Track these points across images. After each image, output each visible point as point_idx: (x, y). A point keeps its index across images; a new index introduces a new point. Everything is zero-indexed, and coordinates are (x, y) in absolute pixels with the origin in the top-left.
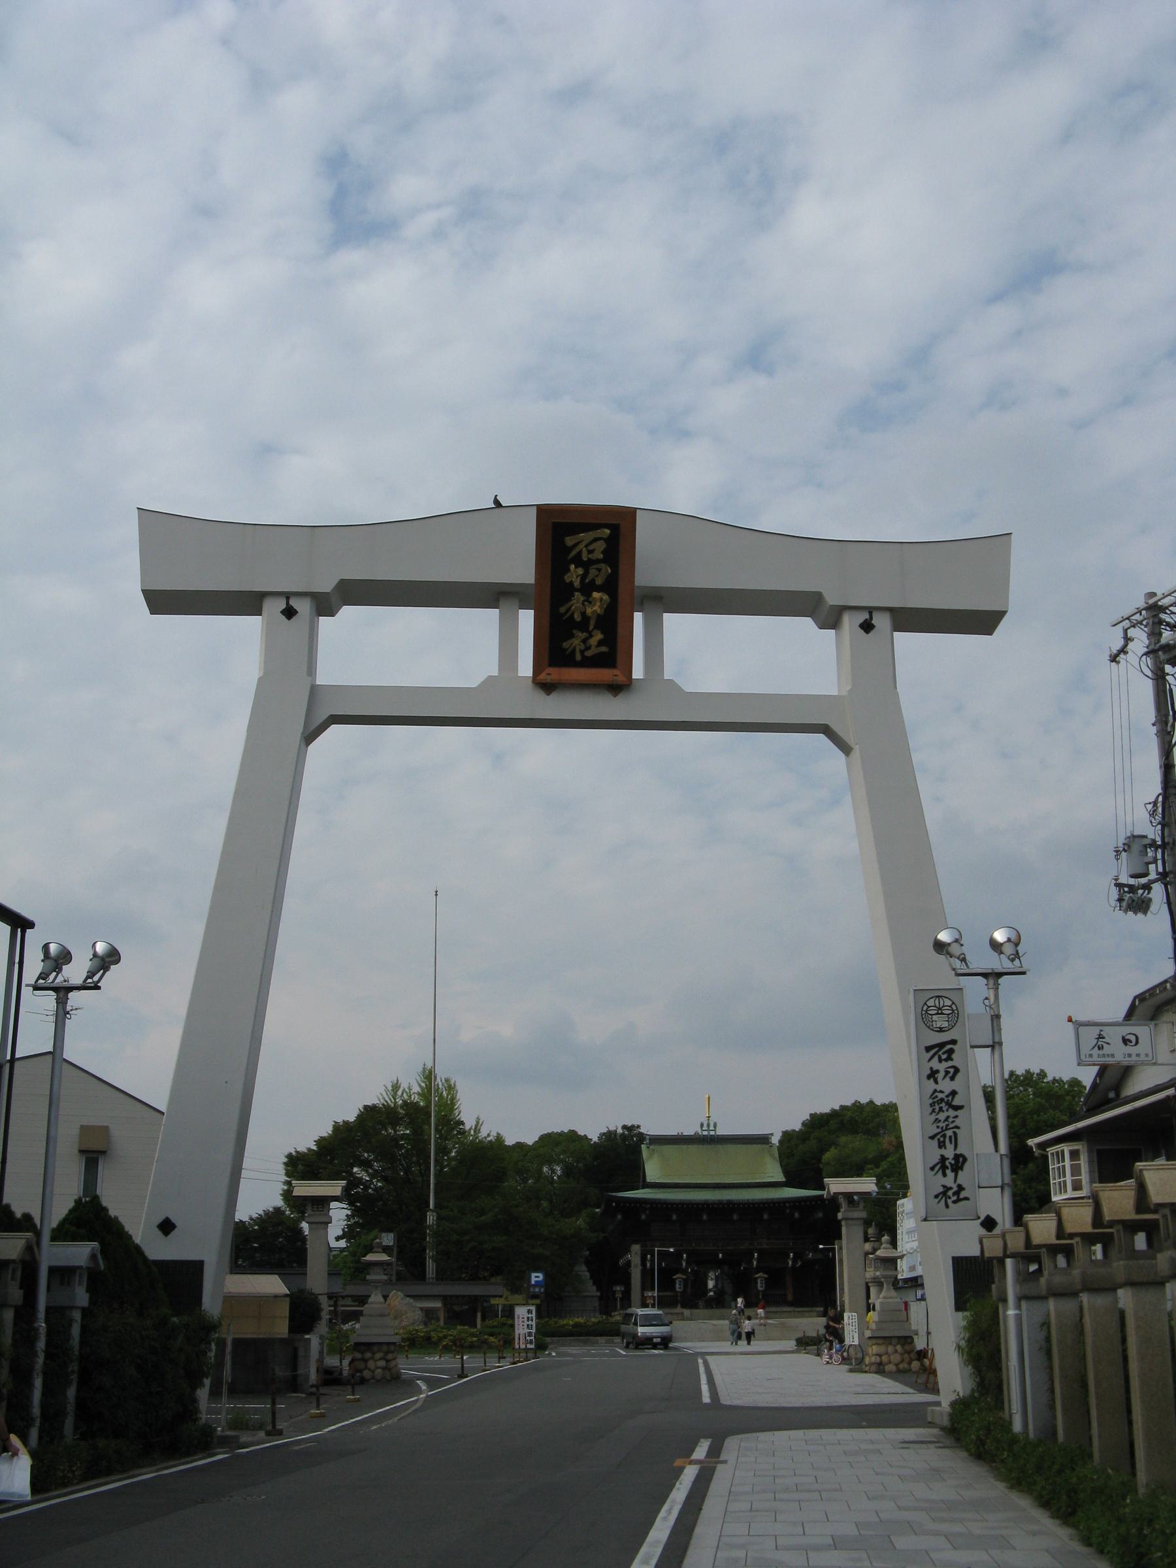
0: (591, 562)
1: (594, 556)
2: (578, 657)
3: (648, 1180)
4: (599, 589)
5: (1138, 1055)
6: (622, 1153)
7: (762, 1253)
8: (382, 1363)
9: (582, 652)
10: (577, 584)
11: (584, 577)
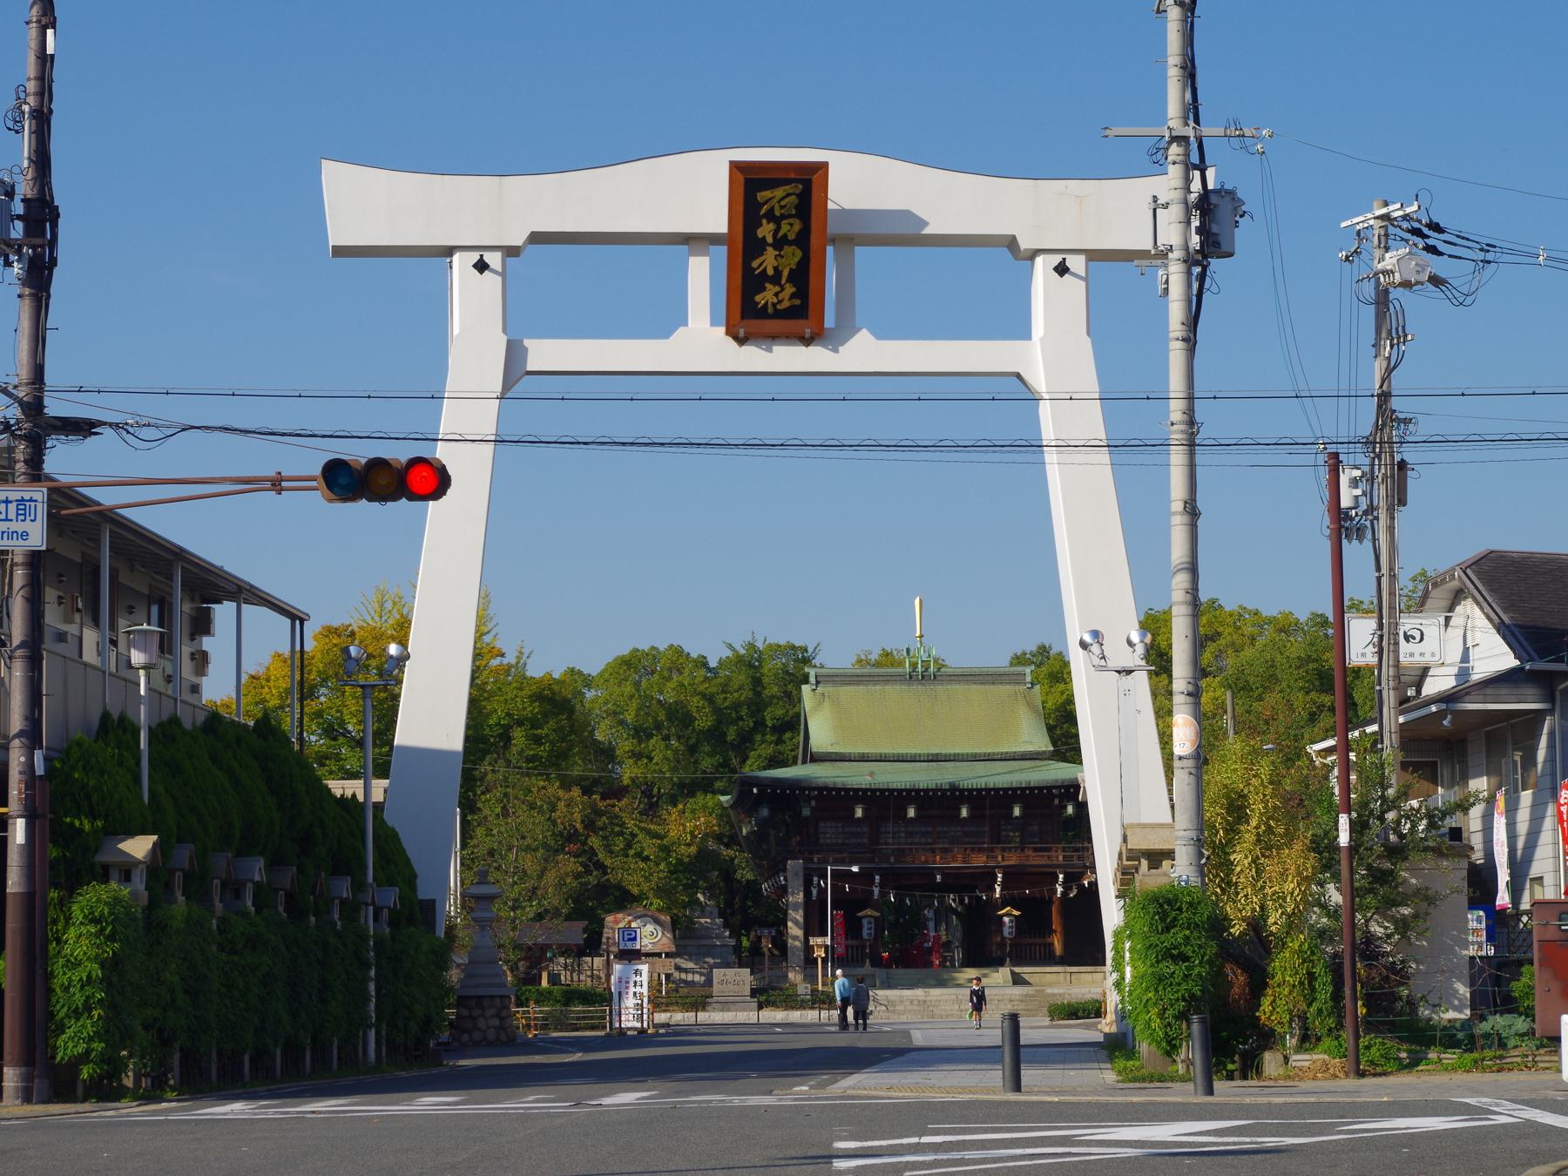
0: (783, 217)
2: (770, 310)
4: (791, 243)
5: (1422, 654)
6: (753, 704)
7: (1012, 877)
8: (496, 1022)
10: (770, 240)
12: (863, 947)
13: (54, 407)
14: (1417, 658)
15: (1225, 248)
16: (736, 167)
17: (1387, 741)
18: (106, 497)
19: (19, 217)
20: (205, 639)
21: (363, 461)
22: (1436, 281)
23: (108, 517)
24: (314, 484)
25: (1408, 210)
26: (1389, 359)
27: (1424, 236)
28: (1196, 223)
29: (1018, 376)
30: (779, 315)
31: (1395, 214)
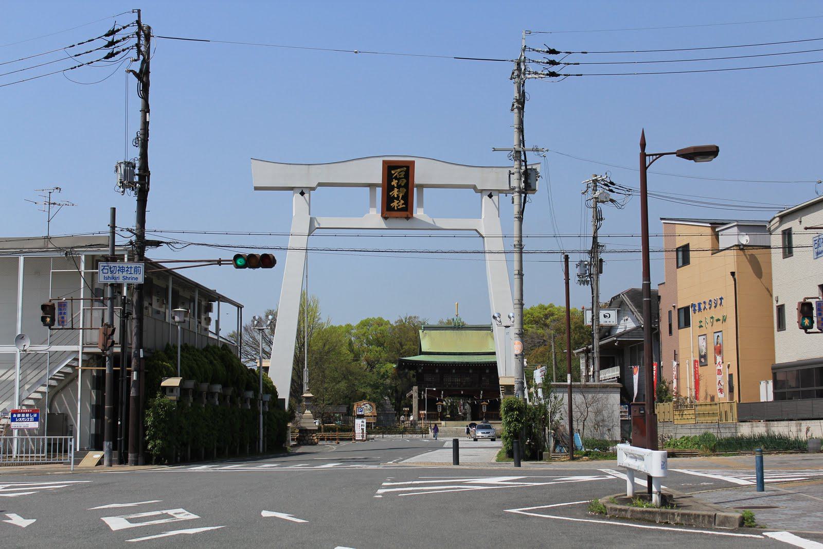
1: (400, 177)
2: (396, 208)
3: (423, 350)
4: (403, 187)
6: (407, 335)
9: (397, 207)
10: (396, 186)
11: (397, 183)
12: (438, 414)
13: (148, 237)
14: (608, 323)
15: (533, 187)
16: (384, 162)
17: (595, 350)
18: (168, 266)
19: (137, 175)
20: (210, 313)
21: (247, 255)
22: (612, 201)
23: (170, 272)
24: (231, 262)
25: (603, 178)
26: (597, 226)
27: (609, 186)
28: (523, 179)
29: (476, 230)
30: (399, 210)
31: (599, 179)
